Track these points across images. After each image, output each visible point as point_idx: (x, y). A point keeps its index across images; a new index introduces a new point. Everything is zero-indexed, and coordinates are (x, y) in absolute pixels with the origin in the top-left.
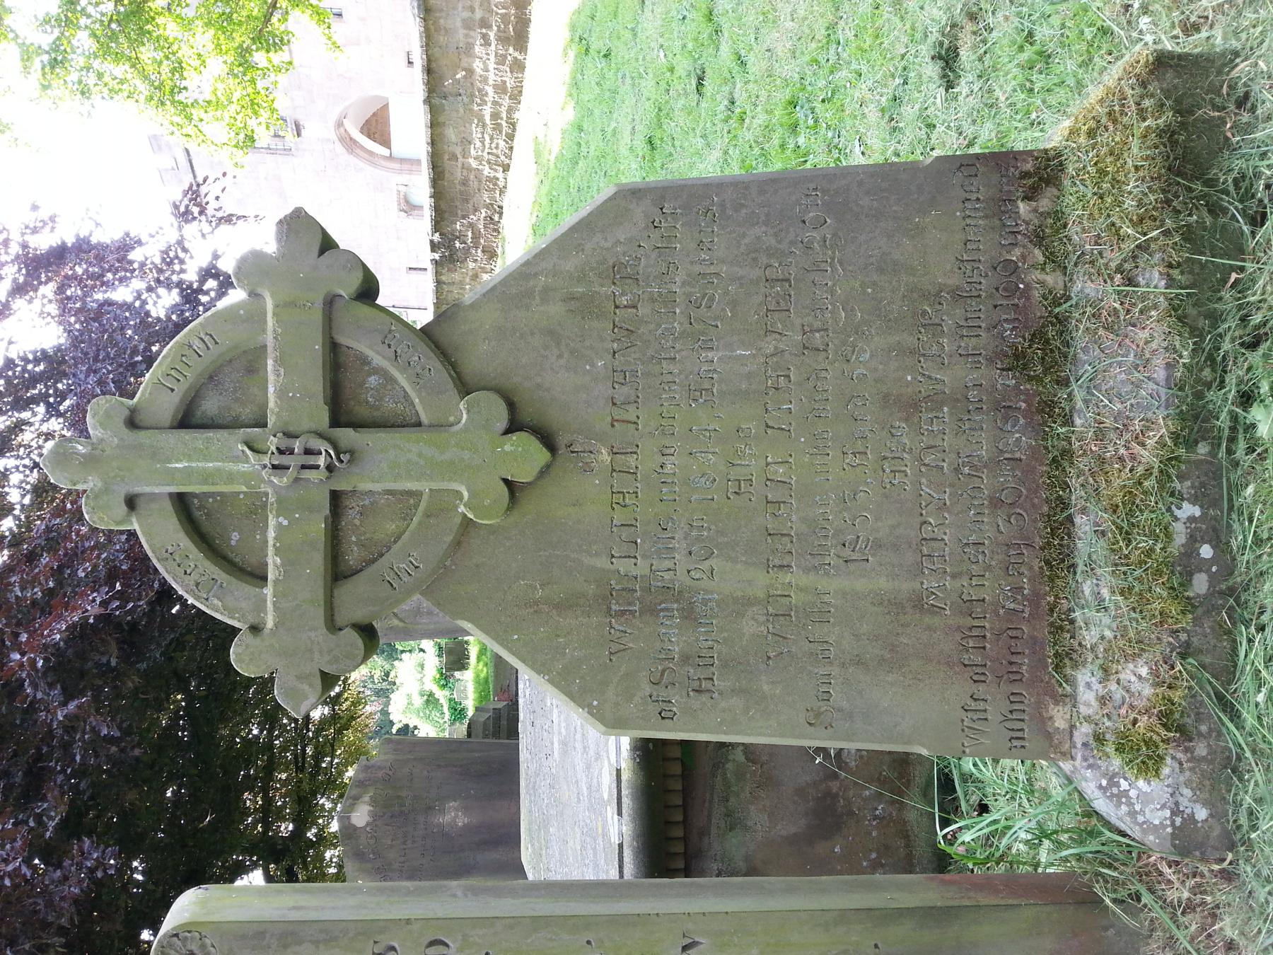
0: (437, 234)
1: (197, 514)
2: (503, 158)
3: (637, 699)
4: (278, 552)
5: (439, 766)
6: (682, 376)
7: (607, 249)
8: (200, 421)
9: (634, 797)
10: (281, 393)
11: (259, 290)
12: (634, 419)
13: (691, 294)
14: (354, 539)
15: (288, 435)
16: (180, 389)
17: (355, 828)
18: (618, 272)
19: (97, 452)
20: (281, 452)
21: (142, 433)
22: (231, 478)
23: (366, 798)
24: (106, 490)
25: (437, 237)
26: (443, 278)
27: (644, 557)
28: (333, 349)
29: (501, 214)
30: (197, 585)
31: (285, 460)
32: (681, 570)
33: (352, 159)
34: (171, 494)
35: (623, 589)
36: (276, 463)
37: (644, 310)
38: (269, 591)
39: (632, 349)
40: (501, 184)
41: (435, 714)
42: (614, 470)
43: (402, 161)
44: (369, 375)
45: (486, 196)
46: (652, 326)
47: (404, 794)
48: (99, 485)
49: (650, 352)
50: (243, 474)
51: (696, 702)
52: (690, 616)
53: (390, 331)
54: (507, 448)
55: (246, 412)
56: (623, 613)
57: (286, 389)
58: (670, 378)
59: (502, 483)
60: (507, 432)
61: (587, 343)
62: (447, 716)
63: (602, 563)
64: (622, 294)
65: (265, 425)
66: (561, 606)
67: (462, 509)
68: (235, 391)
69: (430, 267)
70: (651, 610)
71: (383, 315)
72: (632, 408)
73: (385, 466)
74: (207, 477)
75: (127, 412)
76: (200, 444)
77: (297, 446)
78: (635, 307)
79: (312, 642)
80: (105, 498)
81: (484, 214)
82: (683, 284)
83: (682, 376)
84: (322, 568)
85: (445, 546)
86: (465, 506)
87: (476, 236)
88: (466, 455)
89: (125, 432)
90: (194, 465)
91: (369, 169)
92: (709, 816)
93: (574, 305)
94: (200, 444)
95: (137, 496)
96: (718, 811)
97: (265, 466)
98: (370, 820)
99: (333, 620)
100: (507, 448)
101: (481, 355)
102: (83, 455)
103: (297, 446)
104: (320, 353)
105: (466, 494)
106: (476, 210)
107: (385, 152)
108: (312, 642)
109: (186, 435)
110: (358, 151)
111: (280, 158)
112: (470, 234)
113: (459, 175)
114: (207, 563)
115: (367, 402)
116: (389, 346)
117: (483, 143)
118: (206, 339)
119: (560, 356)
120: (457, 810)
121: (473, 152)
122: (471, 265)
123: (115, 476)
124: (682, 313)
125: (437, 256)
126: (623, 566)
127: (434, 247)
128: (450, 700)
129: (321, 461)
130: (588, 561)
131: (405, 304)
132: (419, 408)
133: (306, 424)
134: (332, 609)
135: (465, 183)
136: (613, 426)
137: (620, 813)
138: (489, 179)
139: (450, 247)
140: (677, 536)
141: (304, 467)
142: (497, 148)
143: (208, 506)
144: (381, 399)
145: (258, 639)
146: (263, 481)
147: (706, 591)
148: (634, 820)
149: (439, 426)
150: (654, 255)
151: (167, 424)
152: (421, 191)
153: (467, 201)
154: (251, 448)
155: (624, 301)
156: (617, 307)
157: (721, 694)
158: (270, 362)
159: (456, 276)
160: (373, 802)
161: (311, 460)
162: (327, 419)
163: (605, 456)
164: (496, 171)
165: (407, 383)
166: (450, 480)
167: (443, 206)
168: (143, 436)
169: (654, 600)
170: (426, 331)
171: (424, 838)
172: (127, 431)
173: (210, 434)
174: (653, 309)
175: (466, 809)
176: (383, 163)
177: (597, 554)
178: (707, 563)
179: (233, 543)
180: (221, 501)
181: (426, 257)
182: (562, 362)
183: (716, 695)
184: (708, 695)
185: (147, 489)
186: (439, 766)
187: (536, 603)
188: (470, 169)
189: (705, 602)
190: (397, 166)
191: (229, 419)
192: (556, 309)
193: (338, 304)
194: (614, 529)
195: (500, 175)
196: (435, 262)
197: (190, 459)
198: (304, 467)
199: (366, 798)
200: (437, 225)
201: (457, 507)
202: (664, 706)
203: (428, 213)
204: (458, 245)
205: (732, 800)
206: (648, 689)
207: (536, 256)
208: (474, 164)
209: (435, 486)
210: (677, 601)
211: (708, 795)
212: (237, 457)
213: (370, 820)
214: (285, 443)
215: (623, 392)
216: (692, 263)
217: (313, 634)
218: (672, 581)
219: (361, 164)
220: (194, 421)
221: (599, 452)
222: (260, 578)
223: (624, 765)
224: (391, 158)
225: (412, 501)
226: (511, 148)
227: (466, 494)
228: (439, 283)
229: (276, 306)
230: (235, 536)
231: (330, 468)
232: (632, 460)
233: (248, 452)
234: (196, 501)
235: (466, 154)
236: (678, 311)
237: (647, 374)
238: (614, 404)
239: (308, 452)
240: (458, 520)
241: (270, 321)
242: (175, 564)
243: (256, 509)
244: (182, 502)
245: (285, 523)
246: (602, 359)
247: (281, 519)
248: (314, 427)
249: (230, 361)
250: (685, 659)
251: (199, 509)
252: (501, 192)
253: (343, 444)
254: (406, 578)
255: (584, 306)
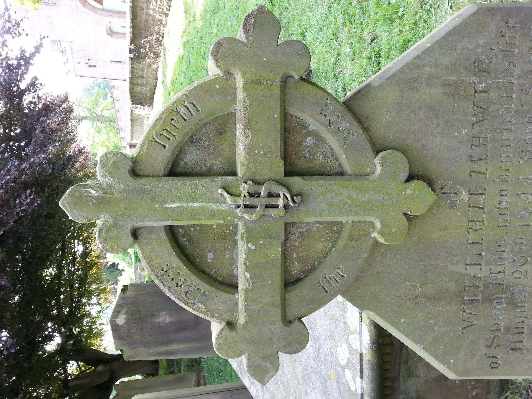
0: (132, 45)
1: (182, 240)
2: (165, 10)
3: (477, 357)
4: (248, 269)
5: (157, 296)
6: (515, 142)
7: (471, 50)
8: (183, 170)
9: (372, 369)
10: (249, 151)
11: (232, 70)
12: (483, 170)
13: (523, 85)
14: (295, 256)
15: (256, 183)
16: (171, 146)
17: (119, 326)
18: (478, 68)
19: (108, 195)
20: (251, 195)
21: (143, 181)
22: (213, 214)
23: (123, 312)
24: (116, 225)
25: (132, 47)
26: (135, 66)
27: (487, 264)
28: (285, 115)
29: (163, 37)
30: (186, 293)
31: (254, 201)
32: (508, 272)
33: (85, 9)
34: (165, 227)
35: (472, 286)
36: (247, 203)
37: (493, 95)
38: (240, 297)
39: (485, 122)
40: (164, 23)
41: (127, 258)
42: (469, 206)
43: (108, 11)
44: (306, 137)
45: (156, 28)
46: (498, 107)
47: (140, 309)
48: (110, 221)
49: (496, 124)
50: (221, 212)
51: (513, 356)
52: (512, 301)
53: (326, 105)
54: (408, 192)
55: (218, 164)
56: (472, 301)
57: (247, 146)
58: (507, 143)
59: (403, 217)
60: (408, 180)
61: (456, 117)
62: (133, 259)
63: (460, 269)
64: (480, 83)
65: (234, 173)
66: (432, 299)
67: (375, 235)
68: (209, 147)
69: (128, 61)
70: (489, 299)
71: (321, 92)
72: (483, 163)
73: (325, 203)
74: (194, 214)
75: (131, 164)
76: (188, 189)
77: (263, 191)
78: (486, 92)
79: (273, 333)
80: (115, 231)
81: (155, 37)
82: (519, 77)
83: (515, 142)
84: (279, 280)
85: (362, 261)
86: (379, 233)
87: (151, 47)
88: (380, 197)
89: (130, 179)
90: (185, 205)
91: (93, 15)
92: (399, 371)
93: (448, 89)
94: (188, 189)
95: (139, 228)
96: (403, 368)
97: (238, 206)
98: (126, 321)
99: (285, 316)
100: (408, 192)
101: (385, 123)
102: (96, 198)
103: (263, 191)
104: (278, 120)
105: (378, 225)
106: (151, 34)
107: (100, 6)
108: (273, 333)
109: (178, 182)
110: (88, 6)
111: (50, 7)
112: (148, 46)
113: (144, 17)
114: (194, 278)
115: (305, 157)
116: (325, 115)
117: (156, 3)
118: (190, 107)
119: (438, 125)
120: (165, 315)
121: (151, 7)
122: (148, 60)
123: (123, 215)
124: (517, 98)
125: (132, 56)
126: (473, 271)
127: (131, 51)
128: (135, 253)
129: (280, 202)
130: (451, 267)
131: (110, 78)
132: (343, 158)
133: (267, 174)
134: (285, 308)
135: (147, 21)
136: (470, 175)
137: (362, 377)
138: (158, 20)
139: (138, 51)
140: (507, 250)
141: (267, 207)
142: (163, 5)
143: (190, 233)
144: (314, 155)
145: (234, 333)
146: (236, 216)
147: (523, 286)
148: (372, 382)
149: (360, 176)
150: (501, 55)
151: (162, 173)
152: (124, 24)
153: (147, 30)
154: (228, 193)
155: (481, 87)
156: (476, 92)
157: (528, 351)
158: (240, 128)
159: (141, 65)
160: (127, 313)
161: (273, 201)
162: (283, 171)
163: (465, 196)
164: (162, 16)
165: (332, 141)
166: (369, 214)
167: (136, 32)
168: (144, 183)
169: (492, 292)
170: (348, 104)
171: (151, 328)
172: (131, 179)
173: (196, 181)
174: (499, 95)
175: (170, 315)
176: (100, 12)
177: (457, 263)
178: (524, 267)
179: (209, 260)
180: (200, 230)
181: (126, 56)
182: (440, 129)
183: (524, 352)
184: (520, 352)
185: (149, 224)
186: (157, 296)
187: (417, 297)
188: (150, 15)
189: (521, 292)
190: (106, 13)
191: (205, 169)
192: (437, 92)
193: (290, 82)
194: (469, 246)
195: (164, 18)
196: (131, 59)
197: (181, 200)
198: (267, 207)
199: (123, 312)
200: (133, 41)
201: (370, 233)
202: (494, 360)
203: (128, 36)
204: (142, 50)
205: (410, 362)
206: (484, 350)
207: (424, 52)
208: (151, 12)
209: (356, 218)
210: (505, 293)
211: (398, 360)
212: (217, 199)
213: (126, 321)
214: (254, 189)
215: (478, 152)
216: (525, 63)
217: (273, 327)
218: (502, 279)
219: (89, 12)
220: (179, 170)
221: (461, 194)
222: (232, 286)
223: (365, 352)
224: (103, 9)
225: (335, 228)
226: (170, 6)
227: (378, 225)
228: (132, 68)
229: (246, 83)
230: (210, 256)
231: (286, 207)
232: (481, 199)
233: (226, 195)
234: (181, 230)
235: (148, 8)
236: (514, 96)
237: (494, 140)
238: (472, 160)
239: (270, 195)
240: (371, 243)
241: (240, 94)
242: (170, 279)
243: (228, 234)
244: (172, 232)
245: (253, 248)
246: (466, 128)
247: (250, 245)
248: (273, 176)
249: (206, 125)
250: (508, 329)
251: (183, 236)
252: (164, 27)
253: (295, 190)
254: (335, 284)
255: (455, 90)
